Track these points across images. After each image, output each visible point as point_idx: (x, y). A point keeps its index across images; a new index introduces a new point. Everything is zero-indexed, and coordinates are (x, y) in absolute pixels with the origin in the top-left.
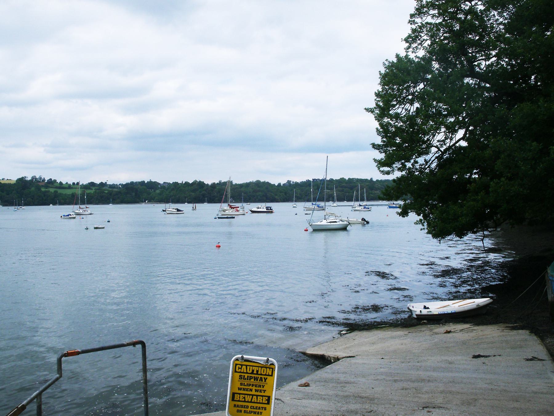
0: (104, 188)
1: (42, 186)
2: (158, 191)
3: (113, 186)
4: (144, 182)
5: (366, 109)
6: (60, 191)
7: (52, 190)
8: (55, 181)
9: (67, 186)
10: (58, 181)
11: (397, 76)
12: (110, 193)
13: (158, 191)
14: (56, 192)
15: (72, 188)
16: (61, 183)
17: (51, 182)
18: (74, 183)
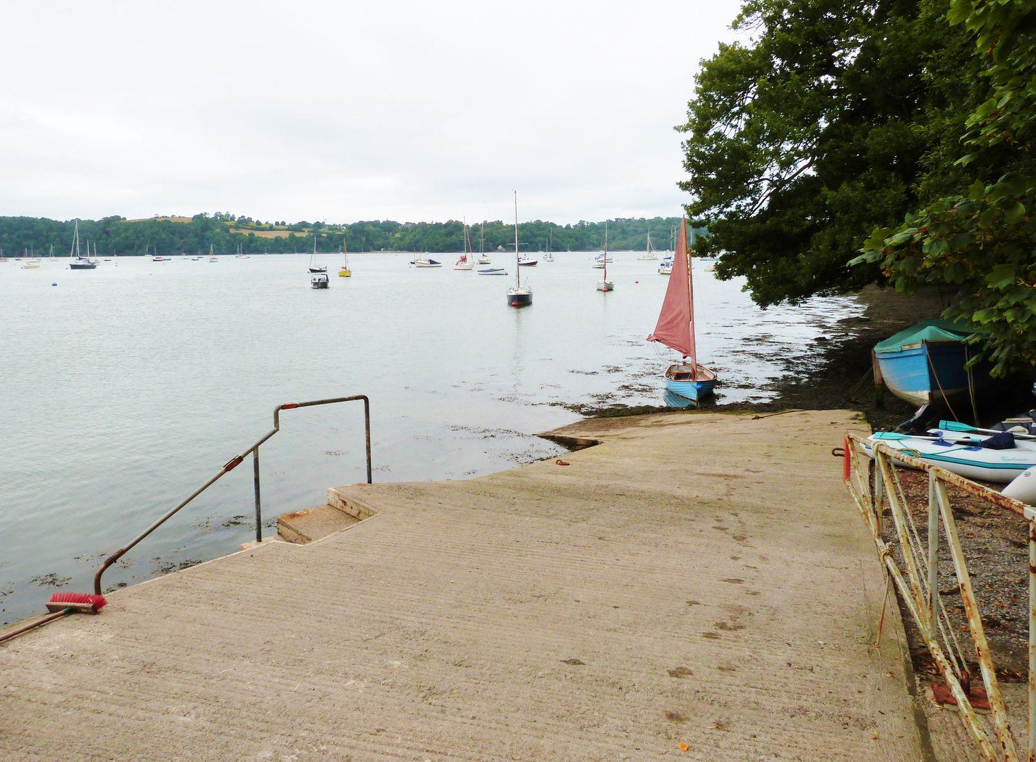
0: (322, 230)
1: (231, 227)
2: (398, 235)
3: (334, 228)
4: (379, 221)
5: (675, 128)
6: (257, 234)
7: (246, 233)
8: (250, 219)
9: (268, 226)
10: (254, 220)
11: (725, 77)
12: (330, 237)
13: (398, 235)
14: (251, 235)
15: (275, 230)
16: (258, 223)
17: (244, 222)
18: (277, 223)
